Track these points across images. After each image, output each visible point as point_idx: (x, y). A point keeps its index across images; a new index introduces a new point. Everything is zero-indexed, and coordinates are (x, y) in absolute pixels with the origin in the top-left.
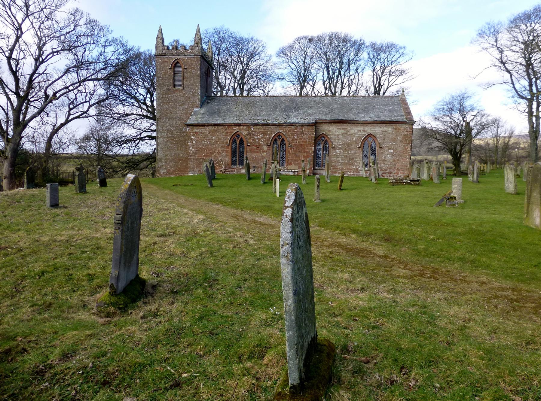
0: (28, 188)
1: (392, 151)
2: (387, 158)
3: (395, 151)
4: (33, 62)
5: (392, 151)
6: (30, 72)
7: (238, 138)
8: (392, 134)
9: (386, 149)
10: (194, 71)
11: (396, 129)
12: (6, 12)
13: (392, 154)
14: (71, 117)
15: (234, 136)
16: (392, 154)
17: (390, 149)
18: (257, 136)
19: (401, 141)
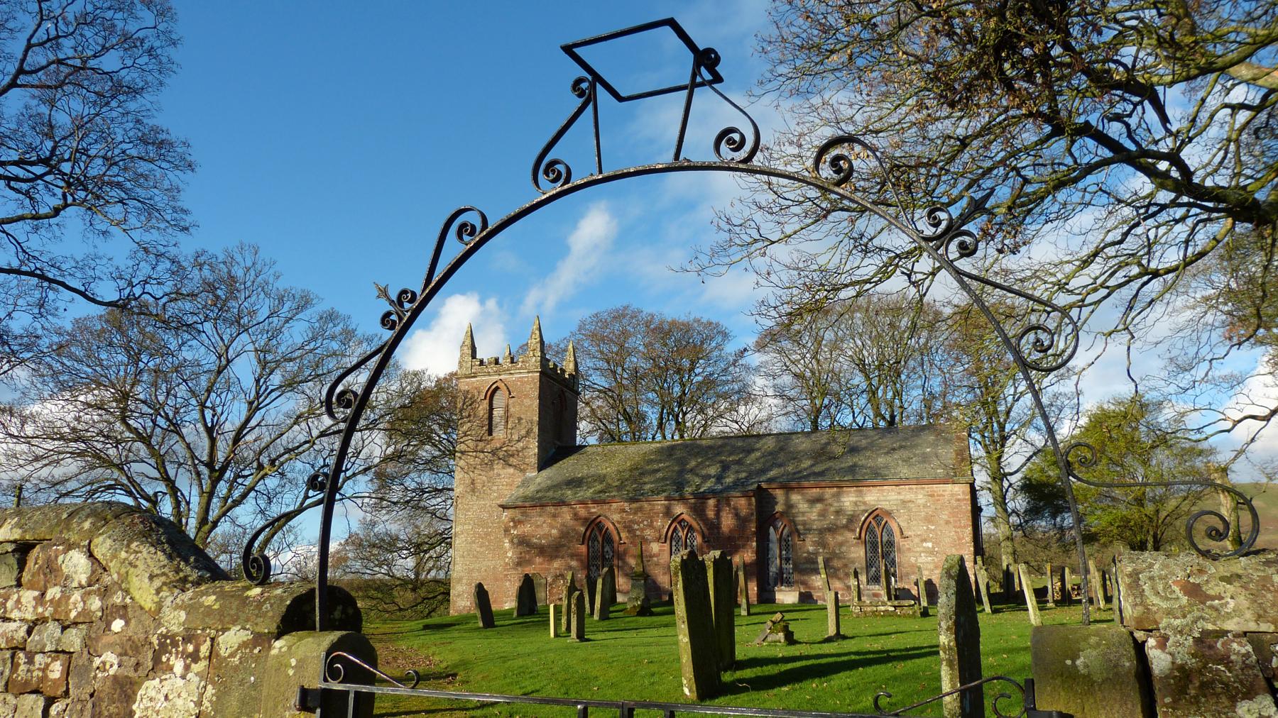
0: (995, 611)
1: (930, 545)
2: (920, 560)
3: (936, 543)
4: (245, 407)
5: (930, 545)
6: (238, 424)
7: (878, 525)
8: (925, 506)
9: (917, 540)
10: (527, 402)
11: (932, 496)
12: (1100, 301)
13: (931, 552)
14: (308, 502)
15: (870, 519)
16: (931, 552)
17: (925, 540)
18: (638, 524)
19: (947, 522)
